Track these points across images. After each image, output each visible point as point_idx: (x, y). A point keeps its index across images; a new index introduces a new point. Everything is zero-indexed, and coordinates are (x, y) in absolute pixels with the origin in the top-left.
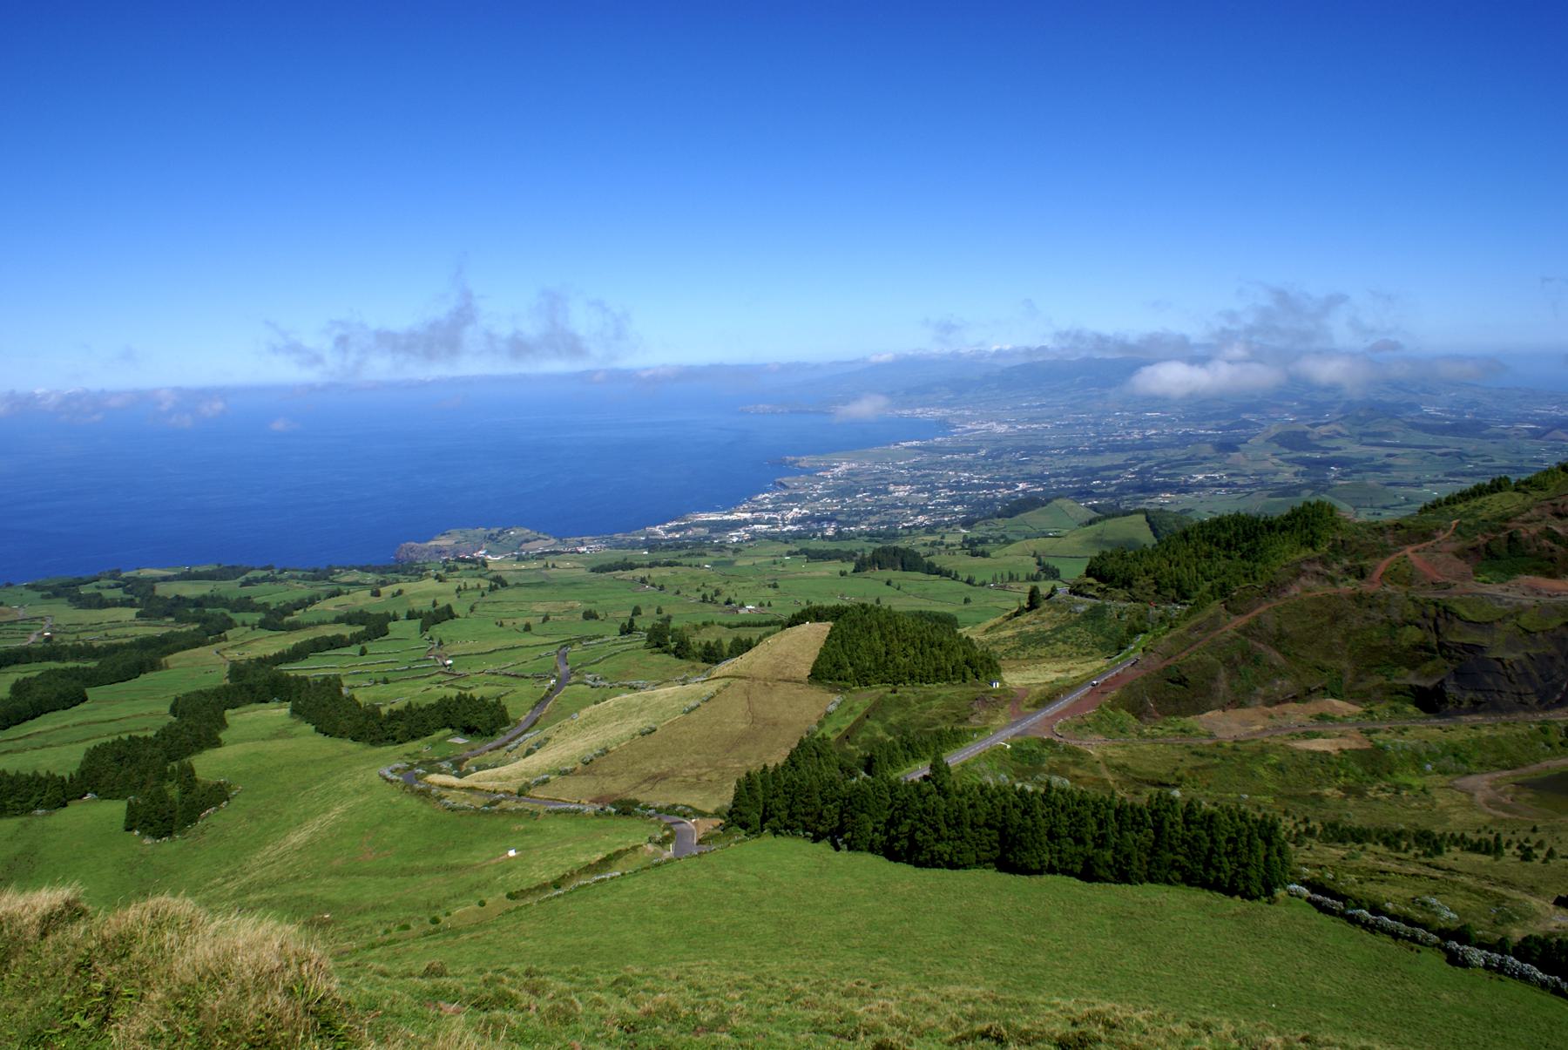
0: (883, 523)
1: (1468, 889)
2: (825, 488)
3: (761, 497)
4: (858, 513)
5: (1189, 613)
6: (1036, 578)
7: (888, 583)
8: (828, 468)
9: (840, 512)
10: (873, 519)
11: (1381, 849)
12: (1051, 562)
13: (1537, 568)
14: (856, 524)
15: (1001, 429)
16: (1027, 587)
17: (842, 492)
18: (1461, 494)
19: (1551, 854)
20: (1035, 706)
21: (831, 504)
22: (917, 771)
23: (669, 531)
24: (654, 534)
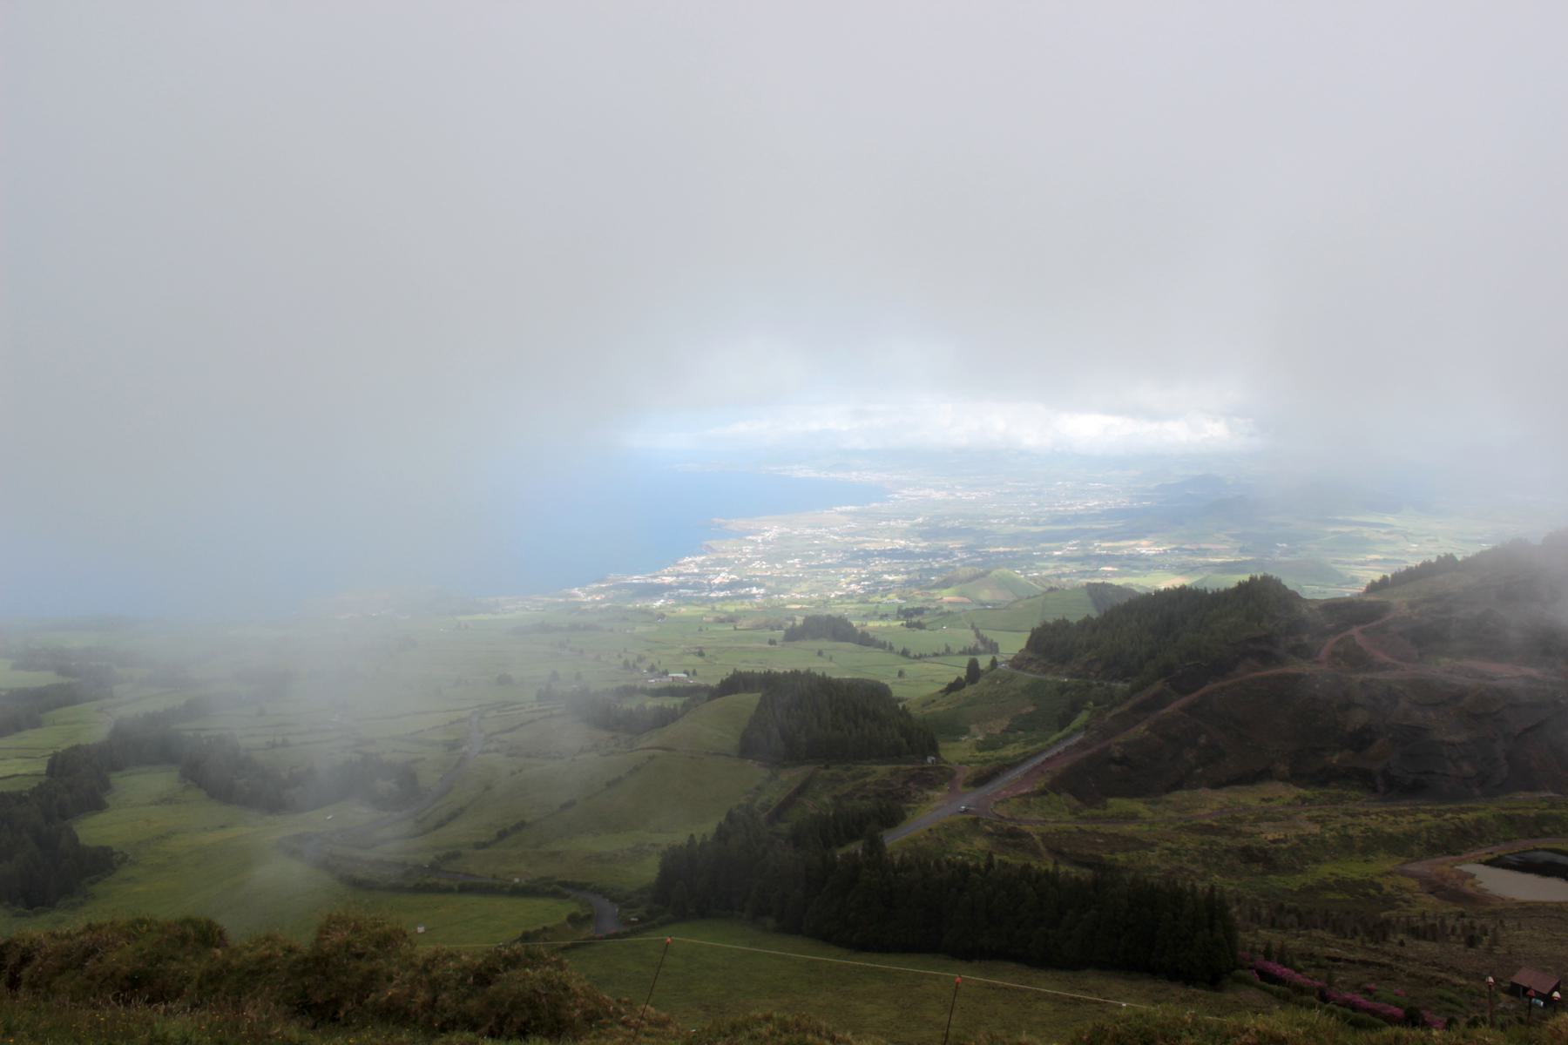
0: (813, 591)
1: (1459, 973)
2: (754, 552)
3: (687, 559)
4: (788, 580)
5: (1133, 691)
6: (974, 651)
7: (820, 653)
8: (758, 532)
9: (771, 578)
10: (804, 587)
11: (1327, 935)
12: (989, 635)
13: (223, 793)
14: (785, 591)
15: (938, 496)
16: (965, 660)
17: (770, 558)
18: (19, 729)
19: (1495, 942)
20: (966, 785)
21: (760, 568)
22: (856, 847)
23: (590, 594)
24: (574, 596)
